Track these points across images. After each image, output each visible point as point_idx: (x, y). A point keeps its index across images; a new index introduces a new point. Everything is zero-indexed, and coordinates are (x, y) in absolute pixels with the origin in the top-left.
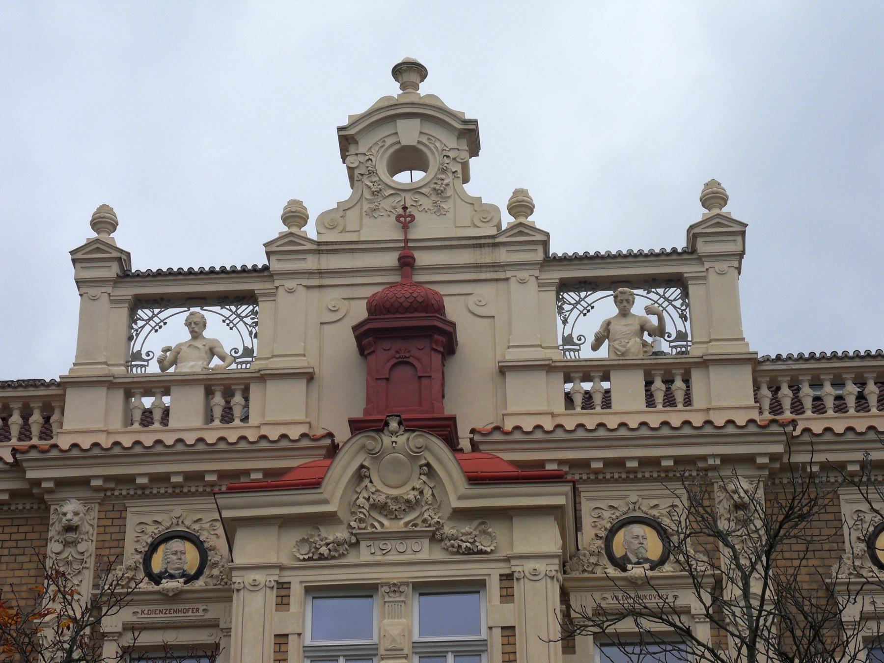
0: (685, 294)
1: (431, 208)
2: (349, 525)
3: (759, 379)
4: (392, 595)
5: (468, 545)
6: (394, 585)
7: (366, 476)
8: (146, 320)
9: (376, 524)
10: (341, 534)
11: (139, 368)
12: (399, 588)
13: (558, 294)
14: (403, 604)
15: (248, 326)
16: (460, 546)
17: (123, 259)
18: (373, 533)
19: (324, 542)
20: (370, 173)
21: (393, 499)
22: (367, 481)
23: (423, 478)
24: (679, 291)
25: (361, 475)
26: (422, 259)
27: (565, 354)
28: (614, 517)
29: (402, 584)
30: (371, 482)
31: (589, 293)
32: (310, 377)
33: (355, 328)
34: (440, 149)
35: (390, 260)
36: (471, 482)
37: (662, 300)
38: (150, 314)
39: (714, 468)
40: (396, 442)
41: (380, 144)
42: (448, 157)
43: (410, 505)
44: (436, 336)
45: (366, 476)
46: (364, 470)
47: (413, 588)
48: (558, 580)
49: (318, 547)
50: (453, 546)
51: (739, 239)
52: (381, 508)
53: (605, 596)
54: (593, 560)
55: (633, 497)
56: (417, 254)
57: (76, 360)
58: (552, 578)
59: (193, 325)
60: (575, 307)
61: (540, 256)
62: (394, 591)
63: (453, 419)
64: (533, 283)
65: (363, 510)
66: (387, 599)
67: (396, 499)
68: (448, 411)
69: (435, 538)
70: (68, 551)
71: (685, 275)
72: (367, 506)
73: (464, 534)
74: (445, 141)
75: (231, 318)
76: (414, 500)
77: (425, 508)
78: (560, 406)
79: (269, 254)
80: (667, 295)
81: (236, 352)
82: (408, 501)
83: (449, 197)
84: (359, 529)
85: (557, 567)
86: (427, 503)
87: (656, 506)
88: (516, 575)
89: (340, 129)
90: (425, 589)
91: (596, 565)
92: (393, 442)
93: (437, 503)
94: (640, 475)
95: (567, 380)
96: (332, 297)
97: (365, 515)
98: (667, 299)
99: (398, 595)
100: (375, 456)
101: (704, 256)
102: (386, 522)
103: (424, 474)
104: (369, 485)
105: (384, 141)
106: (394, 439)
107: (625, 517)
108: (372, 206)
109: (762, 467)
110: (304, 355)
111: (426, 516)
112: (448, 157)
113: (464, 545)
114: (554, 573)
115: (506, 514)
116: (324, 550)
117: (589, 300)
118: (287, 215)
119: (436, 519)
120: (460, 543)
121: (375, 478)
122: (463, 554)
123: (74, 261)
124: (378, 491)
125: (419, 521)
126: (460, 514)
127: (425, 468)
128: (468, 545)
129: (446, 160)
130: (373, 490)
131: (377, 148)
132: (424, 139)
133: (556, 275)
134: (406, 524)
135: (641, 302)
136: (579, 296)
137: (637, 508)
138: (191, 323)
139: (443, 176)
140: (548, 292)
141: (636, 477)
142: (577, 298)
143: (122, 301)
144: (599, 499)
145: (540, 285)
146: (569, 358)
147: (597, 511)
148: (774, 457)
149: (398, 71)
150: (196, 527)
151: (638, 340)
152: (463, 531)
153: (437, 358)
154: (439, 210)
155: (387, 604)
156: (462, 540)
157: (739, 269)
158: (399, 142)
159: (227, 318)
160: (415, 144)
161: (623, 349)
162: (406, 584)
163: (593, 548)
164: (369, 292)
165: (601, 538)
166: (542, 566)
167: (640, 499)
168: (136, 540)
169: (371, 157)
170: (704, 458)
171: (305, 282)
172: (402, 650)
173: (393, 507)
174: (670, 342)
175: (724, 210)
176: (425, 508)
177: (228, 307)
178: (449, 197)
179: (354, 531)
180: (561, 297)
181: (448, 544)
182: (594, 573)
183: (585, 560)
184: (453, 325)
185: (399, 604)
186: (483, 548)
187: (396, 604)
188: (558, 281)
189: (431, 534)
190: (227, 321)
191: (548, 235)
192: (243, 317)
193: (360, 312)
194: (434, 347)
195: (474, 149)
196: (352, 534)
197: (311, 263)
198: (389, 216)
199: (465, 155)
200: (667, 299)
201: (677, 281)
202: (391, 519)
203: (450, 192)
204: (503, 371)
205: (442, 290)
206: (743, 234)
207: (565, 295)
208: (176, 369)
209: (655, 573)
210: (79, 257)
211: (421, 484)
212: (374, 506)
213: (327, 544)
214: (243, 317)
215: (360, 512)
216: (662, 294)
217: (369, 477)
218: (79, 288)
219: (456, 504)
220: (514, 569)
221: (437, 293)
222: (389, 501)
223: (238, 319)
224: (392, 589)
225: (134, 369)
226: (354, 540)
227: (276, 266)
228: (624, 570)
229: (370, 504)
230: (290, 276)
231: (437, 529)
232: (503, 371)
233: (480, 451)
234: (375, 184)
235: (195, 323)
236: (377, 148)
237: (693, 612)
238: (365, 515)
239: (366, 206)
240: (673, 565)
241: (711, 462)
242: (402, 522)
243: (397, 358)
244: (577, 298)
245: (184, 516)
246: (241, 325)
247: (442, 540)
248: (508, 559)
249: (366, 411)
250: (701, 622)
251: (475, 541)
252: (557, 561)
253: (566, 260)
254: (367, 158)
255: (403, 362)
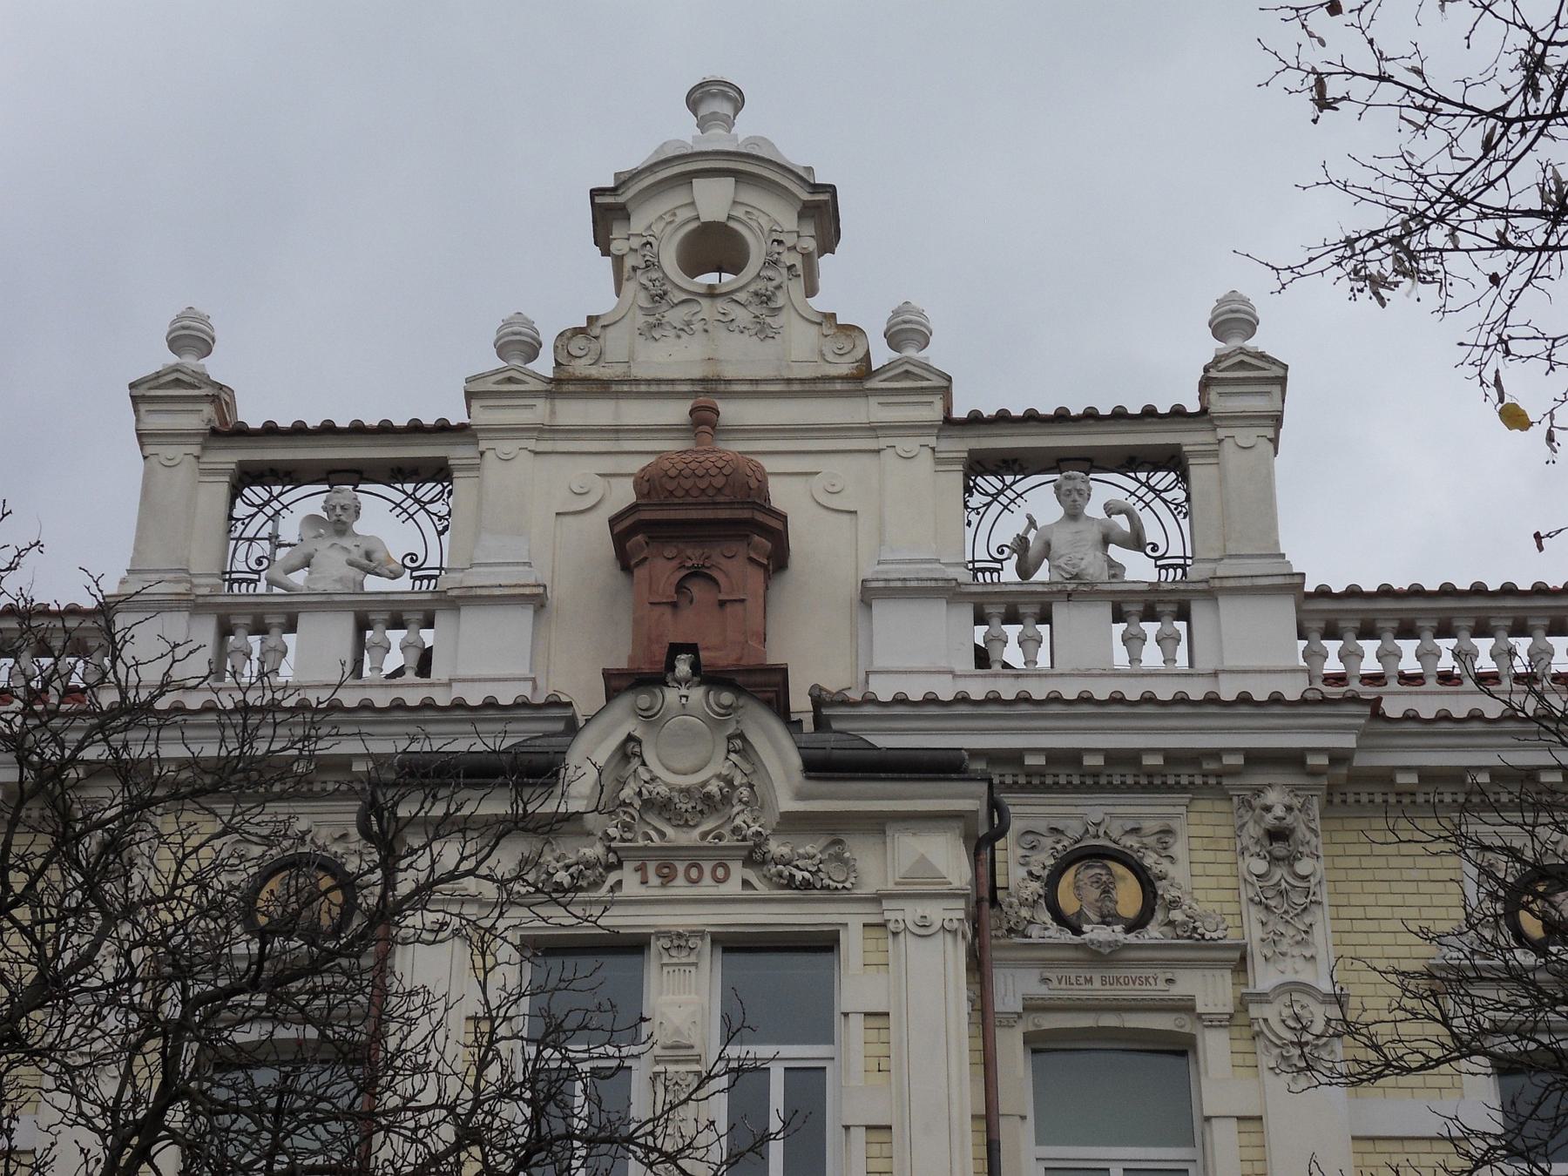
0: (1184, 477)
1: (750, 326)
2: (606, 833)
3: (1307, 624)
4: (673, 952)
5: (807, 875)
6: (679, 935)
7: (635, 755)
8: (257, 506)
9: (653, 833)
10: (594, 851)
11: (244, 585)
12: (687, 941)
13: (967, 477)
14: (693, 969)
15: (435, 518)
16: (792, 876)
17: (220, 397)
18: (646, 848)
19: (561, 864)
20: (649, 266)
21: (681, 791)
22: (635, 762)
23: (733, 756)
24: (1173, 476)
25: (628, 751)
26: (731, 412)
27: (975, 577)
28: (1059, 847)
29: (694, 934)
30: (644, 764)
31: (1018, 477)
32: (537, 601)
33: (613, 521)
34: (766, 229)
35: (677, 412)
36: (812, 774)
37: (1144, 490)
38: (266, 496)
39: (1234, 772)
40: (687, 697)
41: (668, 218)
42: (780, 242)
43: (710, 803)
44: (756, 538)
45: (635, 755)
46: (632, 744)
47: (713, 942)
48: (964, 937)
49: (552, 871)
50: (780, 875)
51: (1276, 389)
52: (662, 807)
53: (1047, 974)
54: (1025, 913)
55: (1096, 815)
56: (722, 406)
57: (132, 565)
58: (954, 932)
59: (338, 511)
60: (995, 499)
61: (934, 413)
62: (679, 946)
63: (783, 671)
64: (925, 460)
65: (630, 810)
66: (666, 960)
67: (686, 792)
68: (773, 659)
69: (754, 857)
70: (1279, 872)
71: (1185, 449)
72: (637, 803)
73: (801, 857)
74: (774, 215)
75: (404, 505)
76: (718, 797)
77: (736, 810)
78: (967, 663)
79: (470, 396)
80: (1152, 482)
81: (413, 561)
82: (708, 797)
83: (780, 309)
84: (623, 840)
85: (961, 915)
86: (740, 801)
87: (1135, 831)
88: (891, 926)
89: (595, 193)
90: (732, 944)
91: (1030, 922)
92: (681, 697)
93: (754, 803)
94: (1103, 781)
95: (980, 619)
96: (582, 472)
97: (633, 818)
98: (1152, 489)
99: (684, 953)
100: (649, 717)
101: (1219, 418)
102: (670, 832)
103: (735, 752)
104: (641, 769)
105: (674, 215)
106: (684, 691)
107: (1077, 846)
108: (651, 320)
109: (1315, 773)
110: (529, 564)
111: (738, 821)
112: (780, 242)
113: (799, 875)
114: (956, 924)
115: (878, 824)
116: (563, 877)
117: (1019, 488)
118: (506, 339)
119: (755, 828)
120: (794, 871)
121: (649, 756)
122: (797, 888)
123: (135, 400)
124: (653, 779)
125: (726, 831)
126: (793, 823)
127: (739, 742)
128: (807, 875)
129: (776, 247)
130: (646, 777)
131: (662, 224)
132: (739, 212)
133: (960, 446)
134: (704, 835)
135: (1106, 490)
136: (1003, 481)
137: (1101, 833)
138: (335, 507)
139: (770, 273)
140: (1093, 1055)
141: (1097, 783)
142: (1000, 485)
143: (214, 472)
144: (1035, 816)
145: (938, 461)
146: (981, 580)
147: (1030, 837)
148: (1339, 758)
149: (697, 97)
150: (338, 848)
151: (1099, 554)
152: (801, 851)
153: (755, 577)
154: (761, 331)
155: (665, 969)
156: (797, 867)
157: (1275, 441)
158: (698, 218)
159: (398, 505)
160: (722, 218)
161: (1075, 571)
162: (701, 934)
163: (1026, 894)
164: (637, 465)
165: (1038, 878)
166: (937, 912)
167: (1107, 818)
168: (1022, 861)
169: (651, 239)
170: (1216, 754)
171: (532, 444)
172: (692, 1047)
173: (684, 806)
174: (1157, 559)
175: (1250, 344)
176: (736, 810)
177: (398, 486)
178: (780, 309)
179: (613, 844)
180: (972, 484)
181: (773, 870)
182: (1026, 937)
183: (1011, 912)
184: (783, 518)
185: (687, 969)
186: (831, 883)
187: (682, 968)
188: (966, 455)
189: (745, 853)
190: (399, 510)
191: (949, 379)
192: (426, 503)
193: (623, 495)
194: (753, 555)
195: (829, 238)
196: (609, 849)
197: (539, 412)
198: (679, 337)
199: (810, 244)
200: (1152, 489)
201: (1174, 461)
202: (678, 826)
203: (780, 300)
204: (869, 594)
205: (769, 464)
206: (1282, 381)
207: (979, 480)
208: (308, 580)
209: (1131, 938)
210: (142, 395)
211: (729, 767)
212: (649, 804)
213: (567, 867)
214: (426, 503)
215: (625, 813)
216: (1144, 480)
217: (641, 756)
218: (142, 445)
219: (787, 804)
220: (887, 915)
221: (759, 466)
222: (675, 794)
223: (417, 506)
224: (676, 943)
225: (236, 586)
226: (612, 858)
227: (483, 416)
228: (1077, 931)
229: (642, 801)
230: (510, 435)
231: (756, 845)
232: (869, 594)
233: (829, 729)
234: (657, 283)
235: (342, 508)
236: (662, 224)
237: (1200, 1009)
238: (633, 818)
239: (641, 320)
240: (1162, 929)
241: (1229, 760)
242: (696, 833)
243: (688, 568)
244: (1000, 485)
245: (314, 829)
246: (422, 517)
247: (764, 862)
248: (877, 899)
249: (631, 659)
250: (1215, 1027)
251: (819, 870)
252: (961, 904)
253: (975, 420)
254: (644, 240)
255: (697, 574)
